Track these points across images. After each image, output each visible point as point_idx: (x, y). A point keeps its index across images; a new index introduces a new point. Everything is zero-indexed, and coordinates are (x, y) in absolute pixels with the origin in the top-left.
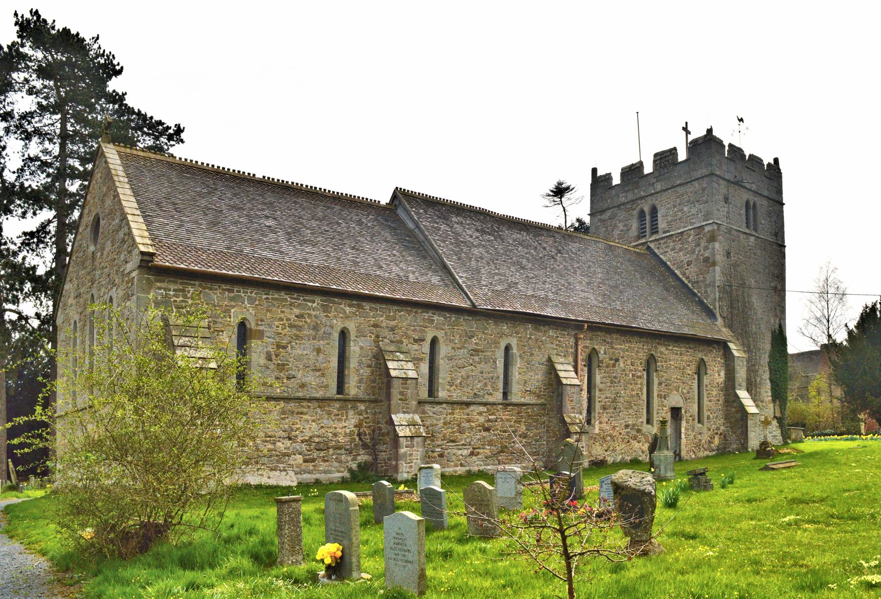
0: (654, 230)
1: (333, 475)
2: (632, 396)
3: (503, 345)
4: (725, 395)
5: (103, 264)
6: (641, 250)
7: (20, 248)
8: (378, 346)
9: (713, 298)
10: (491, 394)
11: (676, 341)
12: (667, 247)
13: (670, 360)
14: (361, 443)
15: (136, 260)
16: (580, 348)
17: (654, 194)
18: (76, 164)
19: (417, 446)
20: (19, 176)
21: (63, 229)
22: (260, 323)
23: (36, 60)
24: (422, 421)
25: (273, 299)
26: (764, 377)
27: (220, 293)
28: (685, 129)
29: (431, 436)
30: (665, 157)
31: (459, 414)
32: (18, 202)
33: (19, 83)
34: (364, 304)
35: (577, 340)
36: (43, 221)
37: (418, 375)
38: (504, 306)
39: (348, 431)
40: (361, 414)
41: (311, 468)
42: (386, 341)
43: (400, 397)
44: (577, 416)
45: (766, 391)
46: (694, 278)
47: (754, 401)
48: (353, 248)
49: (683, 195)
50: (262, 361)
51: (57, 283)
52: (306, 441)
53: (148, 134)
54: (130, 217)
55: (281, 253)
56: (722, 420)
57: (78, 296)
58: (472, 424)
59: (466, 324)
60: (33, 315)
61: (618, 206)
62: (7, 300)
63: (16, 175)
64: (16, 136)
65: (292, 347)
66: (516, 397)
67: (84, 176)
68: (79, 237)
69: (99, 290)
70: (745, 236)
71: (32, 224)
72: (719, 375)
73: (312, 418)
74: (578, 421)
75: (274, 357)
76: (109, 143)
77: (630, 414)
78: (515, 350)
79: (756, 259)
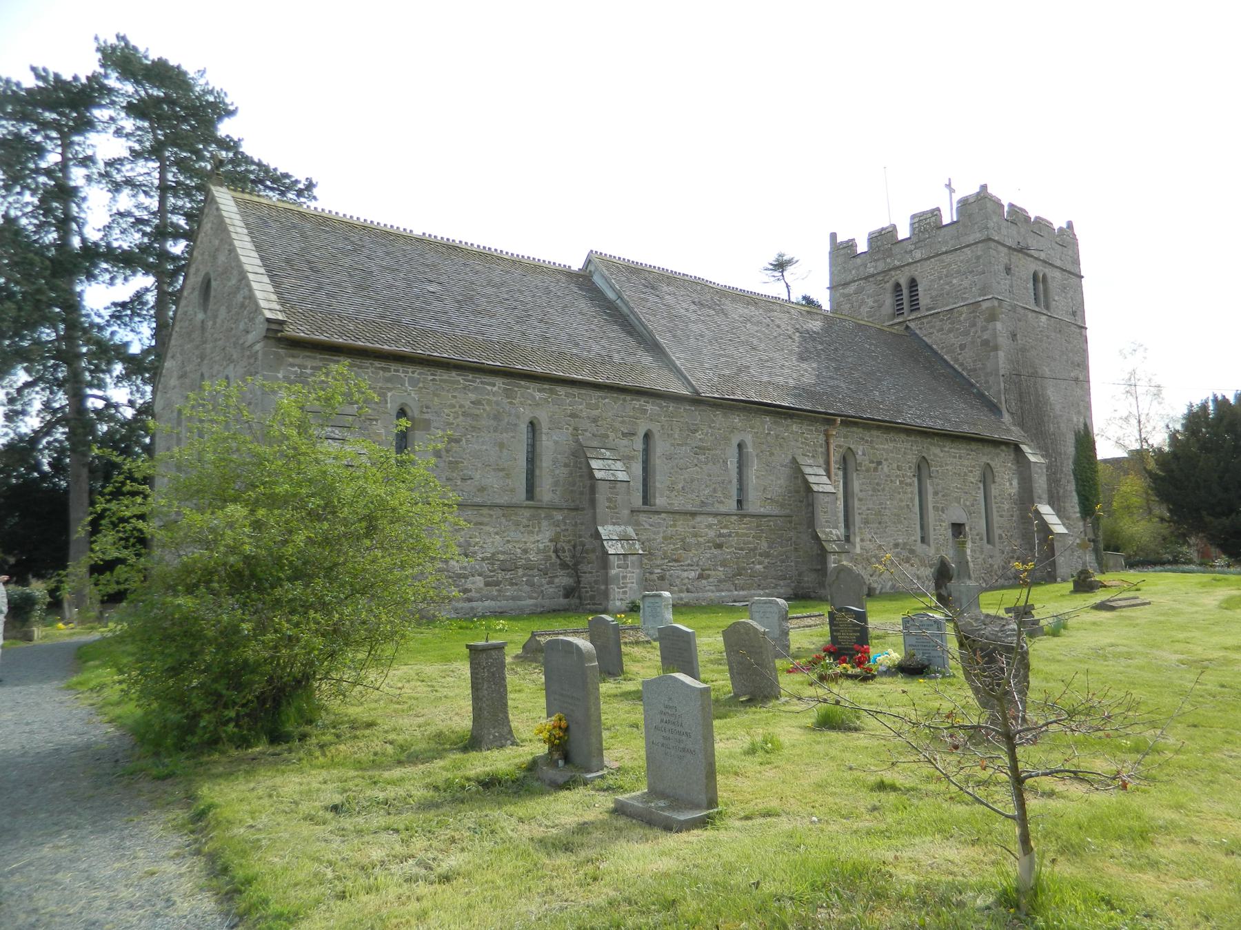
0: (914, 306)
3: (735, 442)
5: (215, 335)
6: (898, 329)
7: (108, 321)
8: (577, 441)
9: (996, 389)
10: (721, 502)
11: (952, 441)
13: (946, 464)
15: (259, 329)
16: (832, 447)
18: (182, 222)
19: (632, 567)
20: (105, 235)
21: (163, 299)
22: (425, 410)
23: (126, 95)
24: (637, 534)
25: (441, 381)
26: (1068, 488)
28: (949, 186)
29: (650, 554)
31: (682, 527)
32: (104, 265)
34: (558, 389)
35: (827, 436)
38: (734, 394)
42: (588, 434)
43: (607, 504)
44: (834, 532)
45: (1073, 504)
48: (541, 321)
49: (950, 264)
52: (487, 559)
53: (272, 189)
54: (251, 276)
55: (449, 324)
57: (183, 376)
58: (700, 539)
59: (688, 415)
60: (126, 402)
61: (866, 278)
62: (91, 385)
64: (101, 186)
65: (467, 441)
66: (755, 504)
70: (1034, 314)
72: (1011, 484)
74: (835, 538)
75: (444, 453)
77: (900, 531)
78: (750, 449)
79: (1050, 344)
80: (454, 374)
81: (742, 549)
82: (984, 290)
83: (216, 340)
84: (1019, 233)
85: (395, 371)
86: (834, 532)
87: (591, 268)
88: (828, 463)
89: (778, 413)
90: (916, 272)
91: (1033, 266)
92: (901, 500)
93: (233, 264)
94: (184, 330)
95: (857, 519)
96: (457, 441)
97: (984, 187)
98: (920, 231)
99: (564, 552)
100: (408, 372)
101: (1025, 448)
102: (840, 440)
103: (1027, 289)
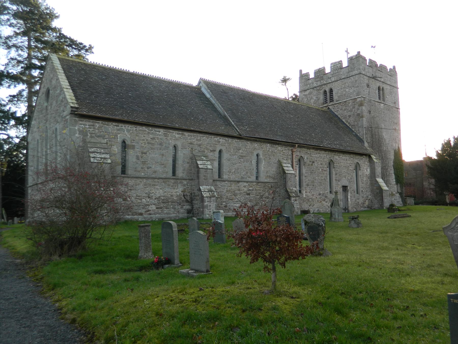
0: (332, 100)
1: (171, 215)
2: (322, 180)
4: (370, 180)
8: (192, 153)
9: (362, 133)
11: (343, 154)
12: (338, 108)
14: (185, 200)
15: (68, 110)
16: (294, 156)
17: (331, 82)
19: (213, 202)
20: (5, 68)
21: (31, 94)
22: (133, 141)
24: (216, 190)
25: (139, 130)
27: (112, 127)
28: (347, 51)
30: (336, 65)
31: (234, 187)
32: (7, 80)
33: (5, 21)
34: (185, 133)
35: (293, 152)
36: (20, 90)
37: (213, 167)
38: (255, 135)
39: (178, 194)
40: (184, 186)
41: (160, 212)
42: (196, 151)
43: (204, 178)
46: (353, 124)
47: (386, 184)
49: (345, 83)
50: (135, 160)
51: (29, 120)
53: (75, 49)
54: (65, 90)
56: (369, 193)
61: (313, 88)
63: (5, 67)
64: (3, 47)
65: (149, 153)
66: (263, 178)
67: (41, 68)
68: (39, 99)
69: (50, 125)
70: (378, 103)
71: (14, 91)
72: (367, 171)
73: (160, 188)
74: (294, 191)
76: (53, 53)
78: (261, 156)
80: (144, 127)
81: (258, 195)
82: (358, 94)
83: (52, 114)
84: (373, 71)
85: (121, 126)
86: (294, 189)
87: (201, 85)
88: (292, 162)
89: (273, 143)
90: (333, 86)
91: (378, 84)
92: (322, 177)
93: (58, 85)
94: (39, 109)
95: (304, 184)
96: (145, 153)
97: (359, 53)
98: (334, 70)
99: (187, 196)
100: (126, 127)
101: (373, 157)
102: (298, 152)
103: (375, 93)
